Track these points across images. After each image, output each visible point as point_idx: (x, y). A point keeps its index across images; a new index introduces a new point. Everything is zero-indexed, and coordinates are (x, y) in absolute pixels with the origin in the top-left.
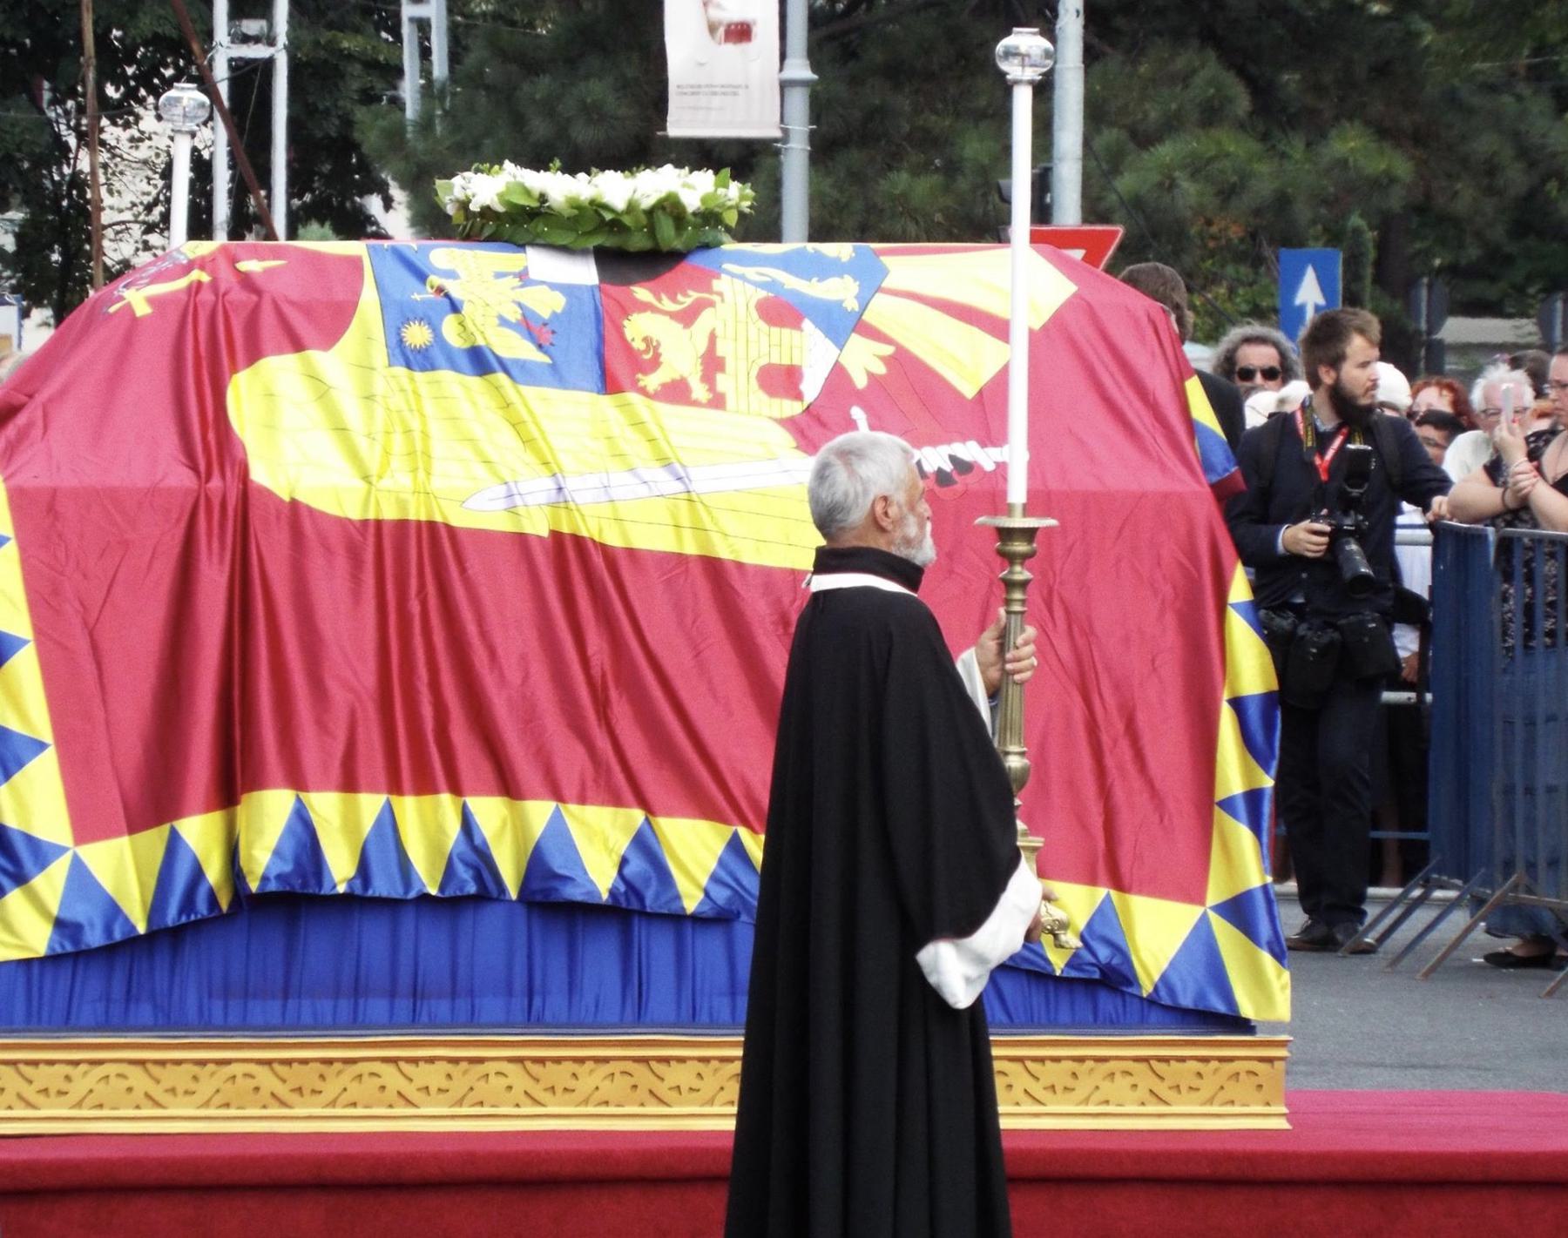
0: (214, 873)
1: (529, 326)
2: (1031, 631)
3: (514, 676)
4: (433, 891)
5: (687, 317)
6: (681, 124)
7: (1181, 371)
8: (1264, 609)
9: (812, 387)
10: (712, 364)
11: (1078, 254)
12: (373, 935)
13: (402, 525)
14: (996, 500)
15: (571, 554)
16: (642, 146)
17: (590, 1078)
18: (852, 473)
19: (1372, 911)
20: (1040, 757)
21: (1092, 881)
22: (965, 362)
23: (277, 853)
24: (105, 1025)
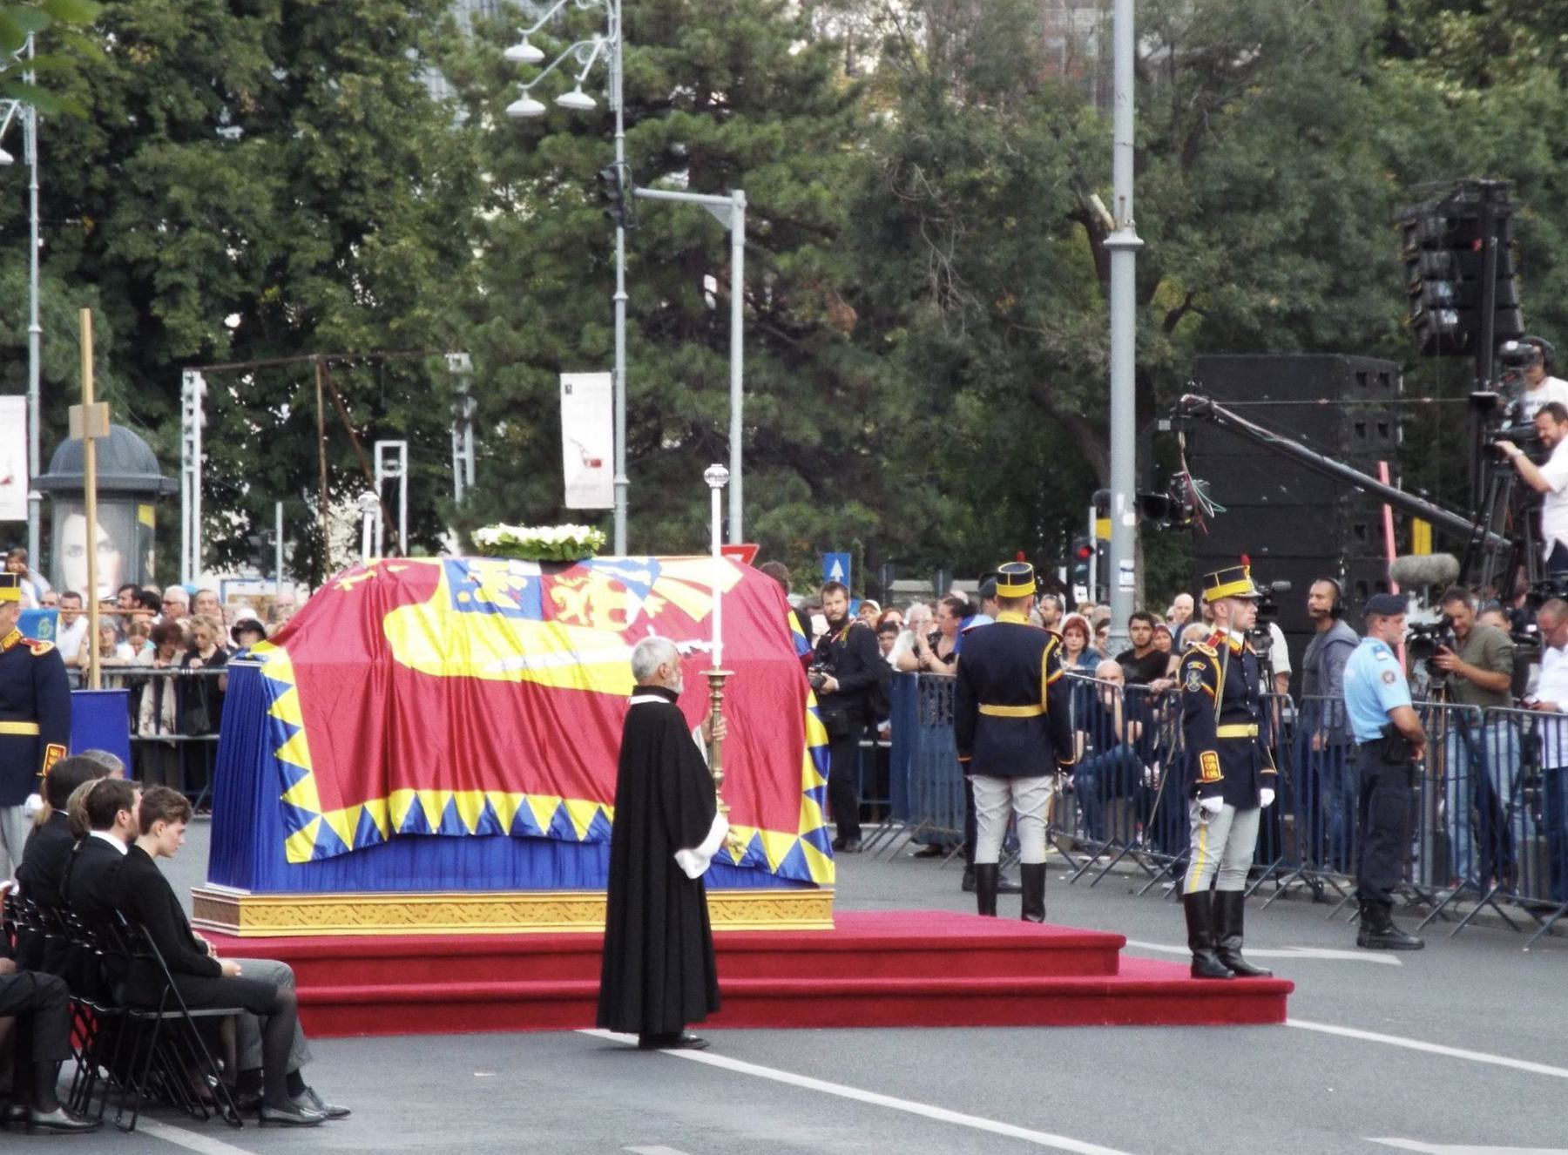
0: (381, 825)
1: (512, 593)
2: (724, 719)
3: (506, 743)
4: (473, 833)
5: (578, 588)
6: (572, 502)
7: (786, 608)
8: (821, 711)
9: (631, 618)
10: (589, 608)
11: (739, 557)
12: (447, 851)
13: (459, 678)
14: (708, 664)
15: (531, 693)
16: (555, 514)
17: (541, 910)
18: (651, 653)
19: (865, 835)
20: (728, 772)
21: (750, 824)
22: (696, 606)
23: (408, 817)
24: (335, 889)
